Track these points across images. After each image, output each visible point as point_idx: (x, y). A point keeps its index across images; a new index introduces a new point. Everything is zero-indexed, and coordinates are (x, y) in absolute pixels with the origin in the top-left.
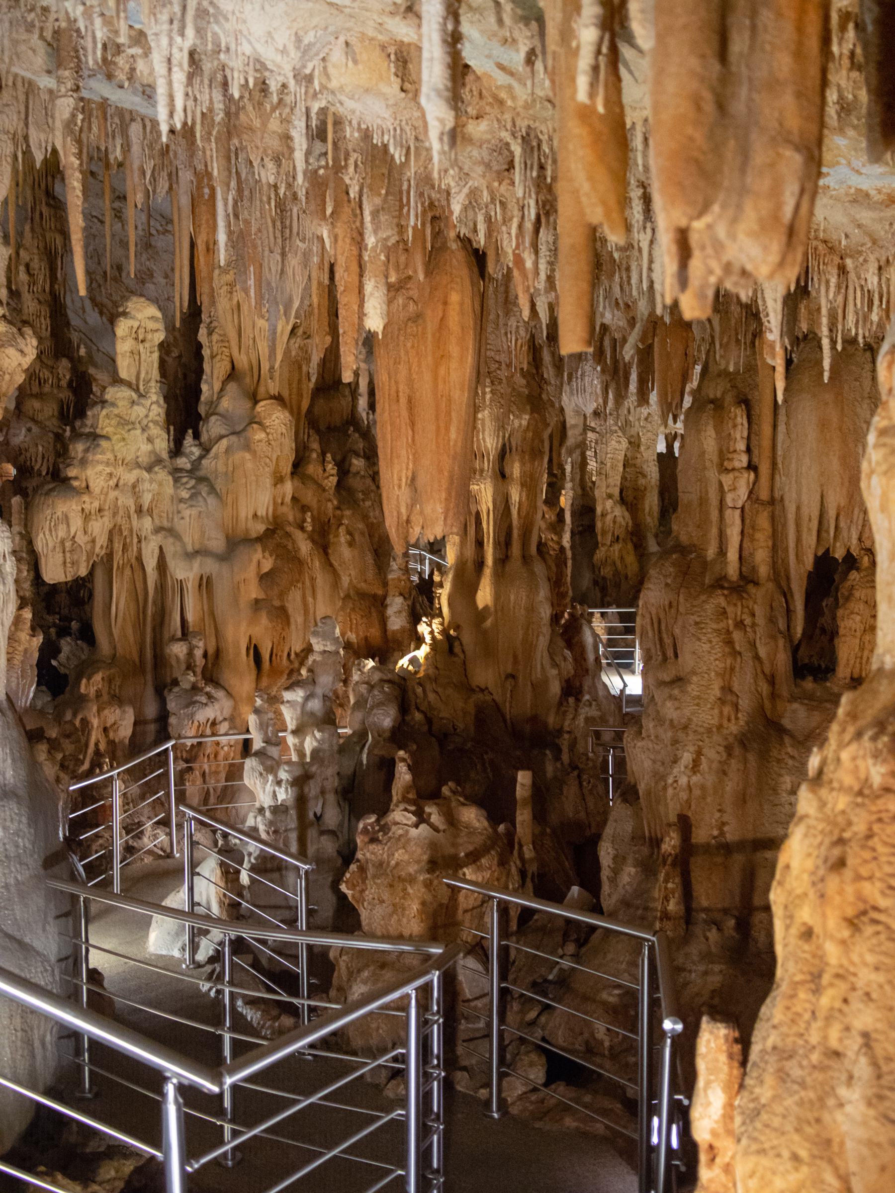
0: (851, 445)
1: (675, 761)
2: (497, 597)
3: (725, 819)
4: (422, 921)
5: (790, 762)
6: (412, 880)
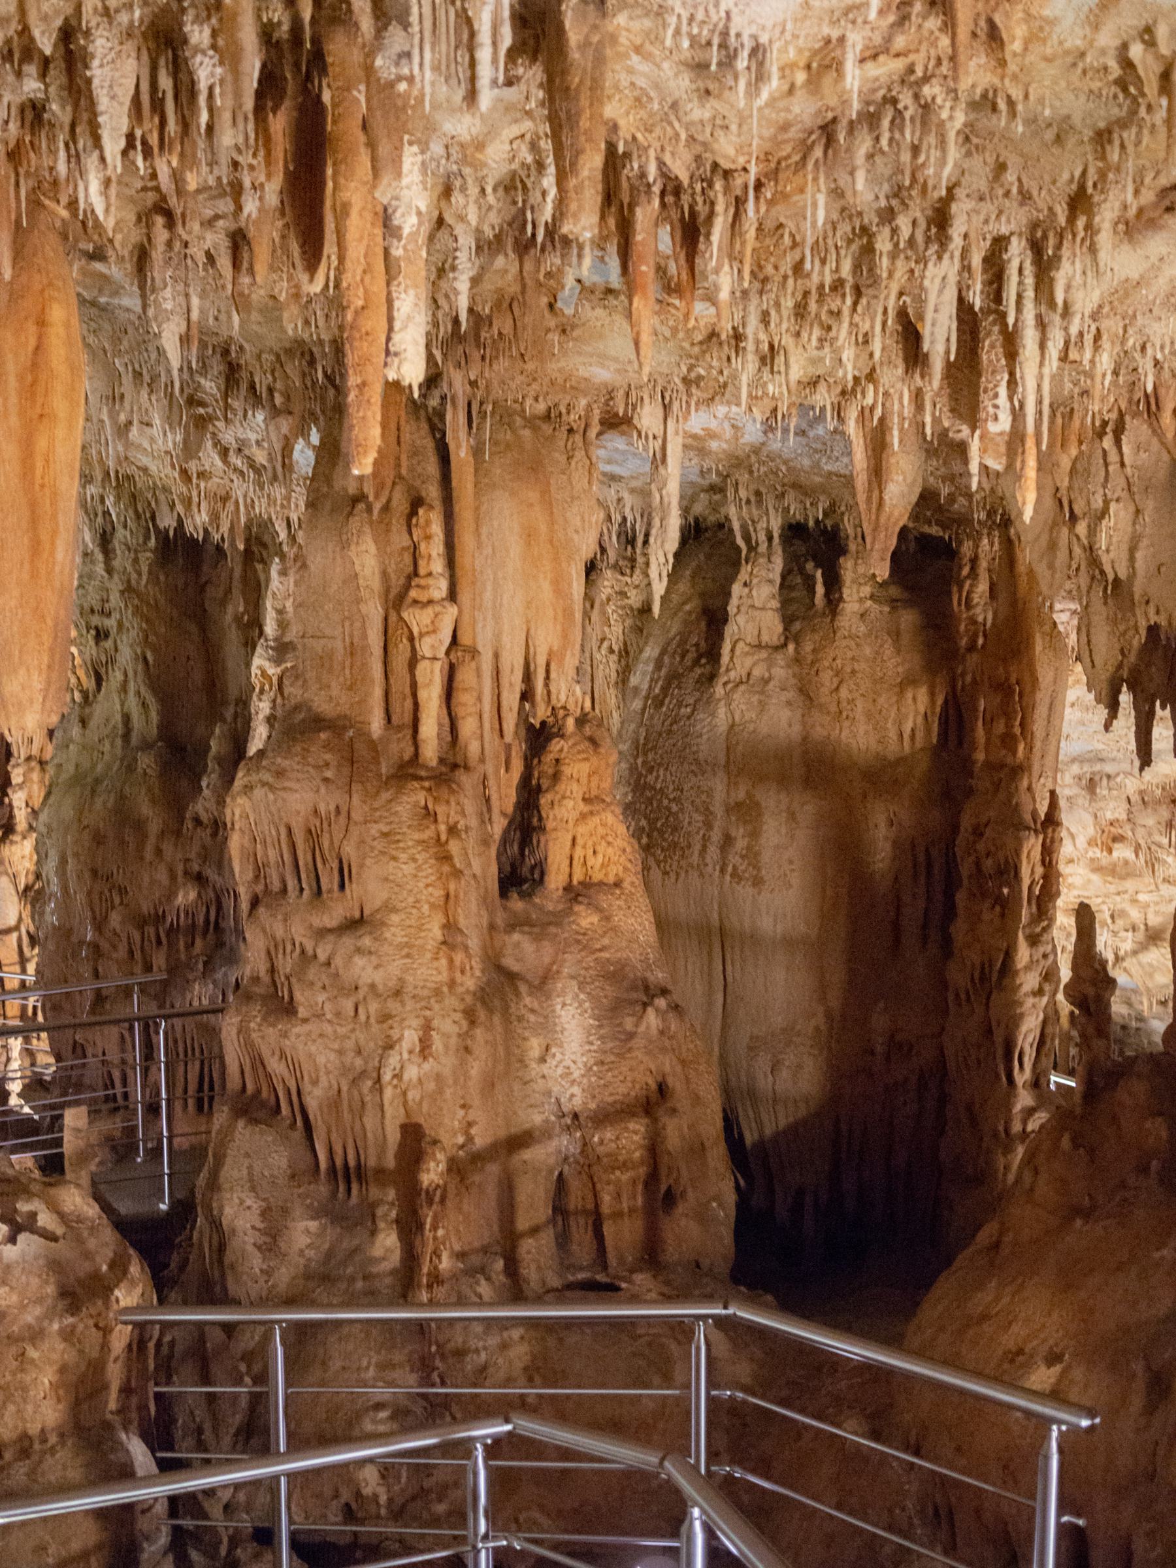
0: (564, 565)
3: (470, 1118)
4: (59, 1400)
5: (532, 1018)
6: (35, 1335)
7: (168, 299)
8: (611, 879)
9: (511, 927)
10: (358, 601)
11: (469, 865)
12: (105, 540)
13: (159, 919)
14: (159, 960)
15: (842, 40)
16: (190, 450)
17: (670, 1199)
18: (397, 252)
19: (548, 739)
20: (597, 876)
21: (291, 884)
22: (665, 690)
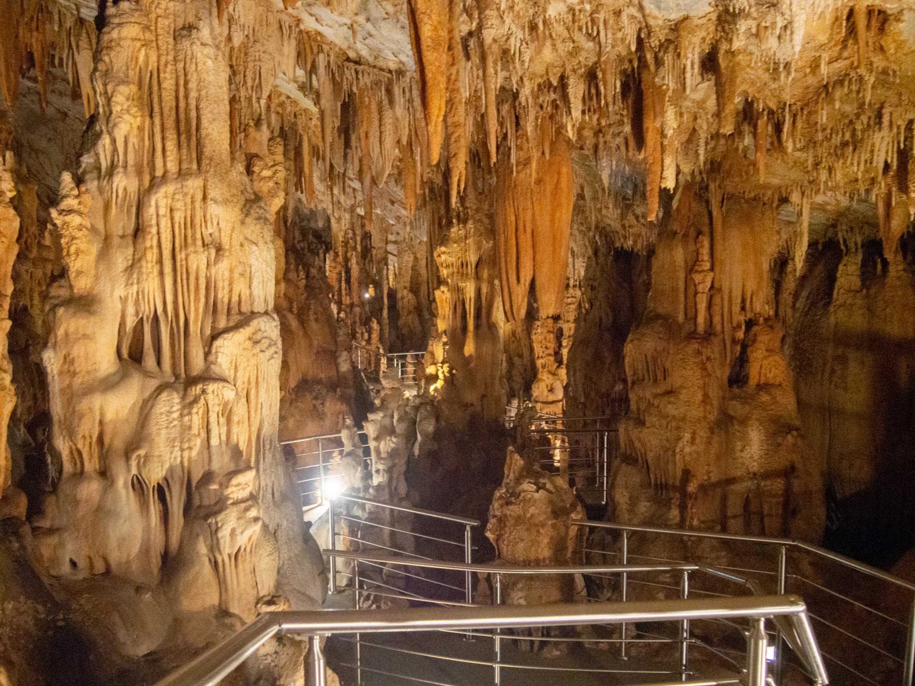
1: (679, 439)
2: (477, 348)
6: (543, 525)
7: (604, 162)
8: (777, 383)
9: (734, 397)
10: (675, 271)
11: (715, 372)
12: (596, 252)
13: (608, 395)
14: (608, 412)
15: (820, 56)
16: (623, 217)
17: (794, 513)
18: (666, 143)
19: (752, 326)
20: (771, 382)
21: (646, 376)
22: (809, 309)
